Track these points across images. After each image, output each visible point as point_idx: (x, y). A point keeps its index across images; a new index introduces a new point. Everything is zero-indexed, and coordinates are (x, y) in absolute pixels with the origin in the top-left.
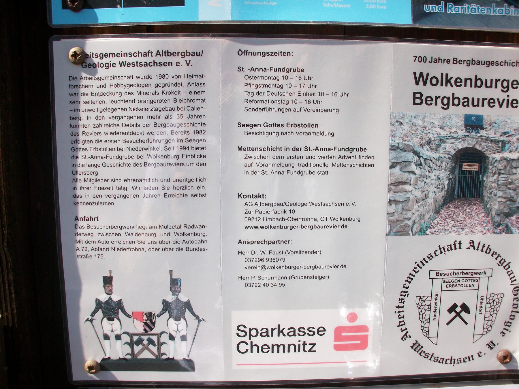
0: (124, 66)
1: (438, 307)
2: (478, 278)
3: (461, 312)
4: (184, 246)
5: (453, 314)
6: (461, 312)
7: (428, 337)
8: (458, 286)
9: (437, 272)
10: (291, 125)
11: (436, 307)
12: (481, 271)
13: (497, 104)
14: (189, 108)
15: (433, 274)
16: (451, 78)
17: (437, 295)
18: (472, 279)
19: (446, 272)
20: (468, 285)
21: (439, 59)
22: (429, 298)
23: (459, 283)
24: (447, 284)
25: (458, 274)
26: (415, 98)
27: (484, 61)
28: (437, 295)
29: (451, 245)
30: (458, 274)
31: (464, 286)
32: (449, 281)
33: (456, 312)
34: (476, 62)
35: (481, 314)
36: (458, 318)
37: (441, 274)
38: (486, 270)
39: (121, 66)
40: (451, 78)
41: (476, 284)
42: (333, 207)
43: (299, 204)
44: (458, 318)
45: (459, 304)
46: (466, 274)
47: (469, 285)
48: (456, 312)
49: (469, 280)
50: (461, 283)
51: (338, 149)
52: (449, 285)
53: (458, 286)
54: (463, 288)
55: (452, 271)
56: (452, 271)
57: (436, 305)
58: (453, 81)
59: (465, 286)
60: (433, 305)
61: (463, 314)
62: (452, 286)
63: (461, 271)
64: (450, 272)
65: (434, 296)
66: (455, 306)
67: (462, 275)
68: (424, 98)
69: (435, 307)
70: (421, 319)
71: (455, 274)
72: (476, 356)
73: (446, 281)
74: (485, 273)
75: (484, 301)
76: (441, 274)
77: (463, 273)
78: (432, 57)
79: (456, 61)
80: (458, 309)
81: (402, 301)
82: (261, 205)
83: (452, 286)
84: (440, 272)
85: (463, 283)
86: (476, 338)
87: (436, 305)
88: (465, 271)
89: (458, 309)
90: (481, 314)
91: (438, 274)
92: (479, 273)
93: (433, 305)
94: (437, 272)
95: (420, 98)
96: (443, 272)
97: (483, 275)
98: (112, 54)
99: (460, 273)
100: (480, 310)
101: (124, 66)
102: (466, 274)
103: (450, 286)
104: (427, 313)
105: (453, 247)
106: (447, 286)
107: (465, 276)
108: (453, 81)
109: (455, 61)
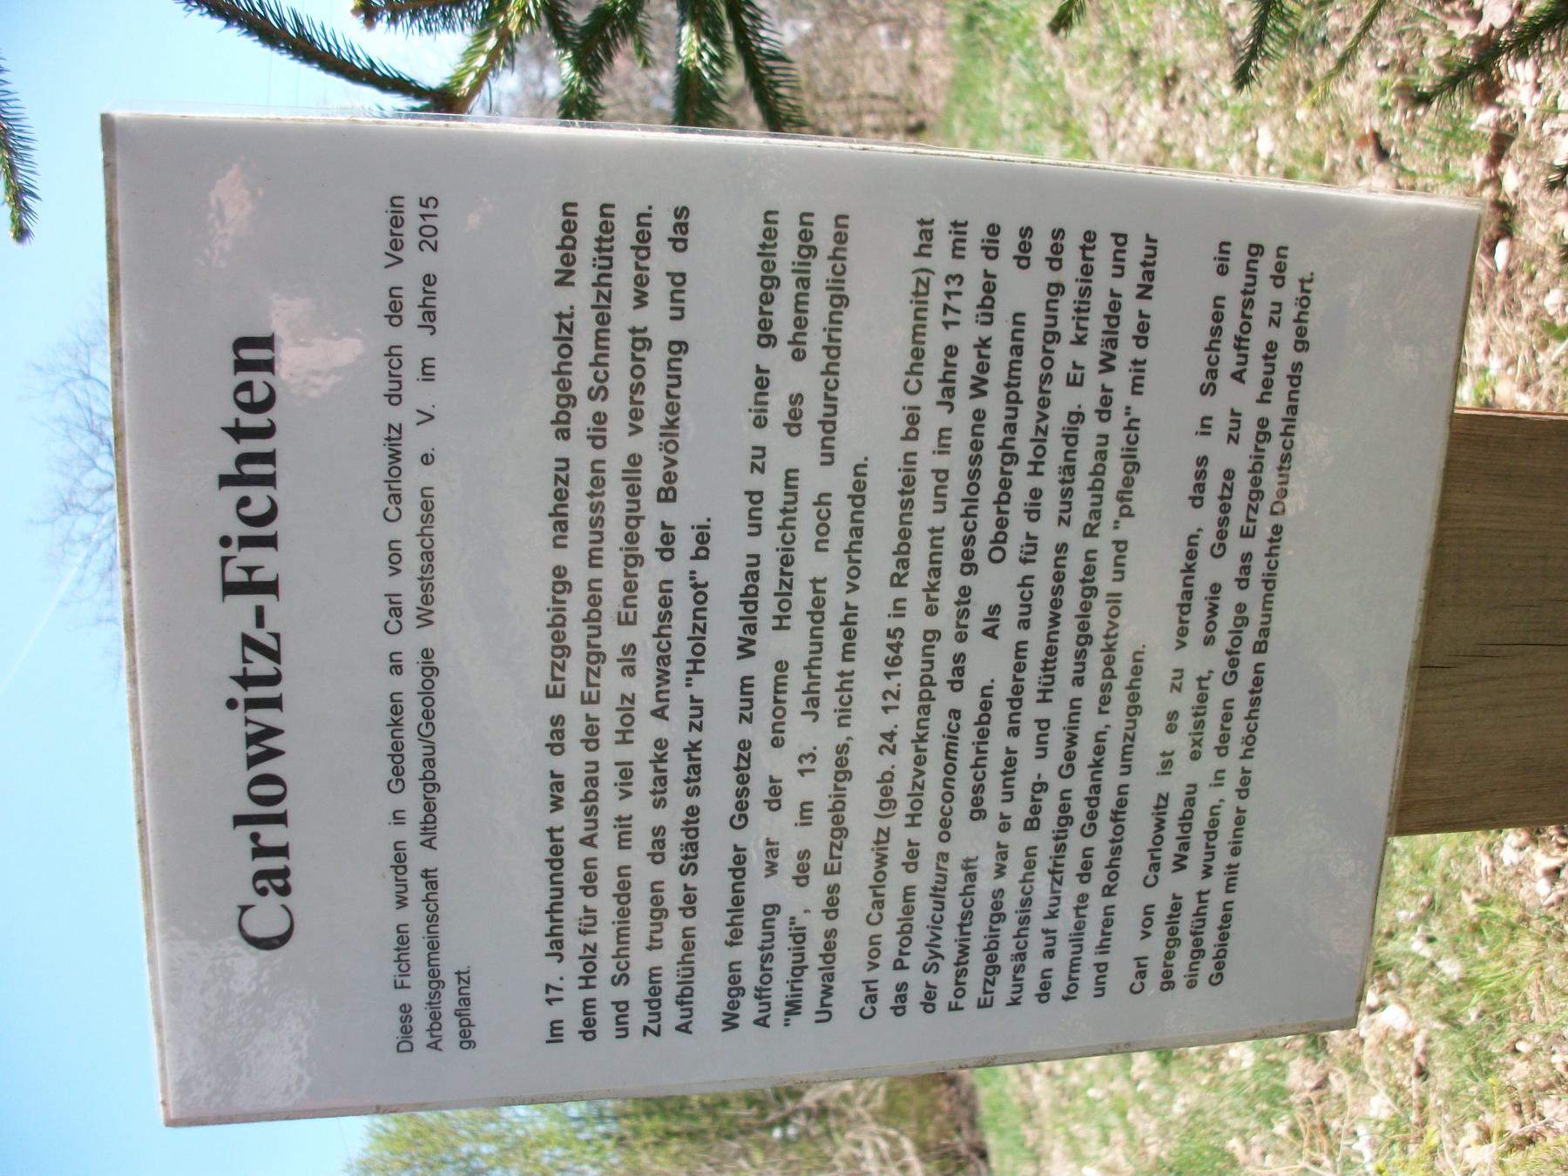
0: (737, 1016)
4: (573, 764)
10: (627, 610)
13: (672, 469)
14: (875, 918)
21: (552, 934)
26: (667, 500)
34: (590, 788)
39: (984, 393)
42: (438, 530)
43: (428, 684)
68: (666, 486)
78: (547, 955)
79: (666, 491)
82: (432, 826)
95: (666, 491)
98: (430, 959)
101: (737, 1016)
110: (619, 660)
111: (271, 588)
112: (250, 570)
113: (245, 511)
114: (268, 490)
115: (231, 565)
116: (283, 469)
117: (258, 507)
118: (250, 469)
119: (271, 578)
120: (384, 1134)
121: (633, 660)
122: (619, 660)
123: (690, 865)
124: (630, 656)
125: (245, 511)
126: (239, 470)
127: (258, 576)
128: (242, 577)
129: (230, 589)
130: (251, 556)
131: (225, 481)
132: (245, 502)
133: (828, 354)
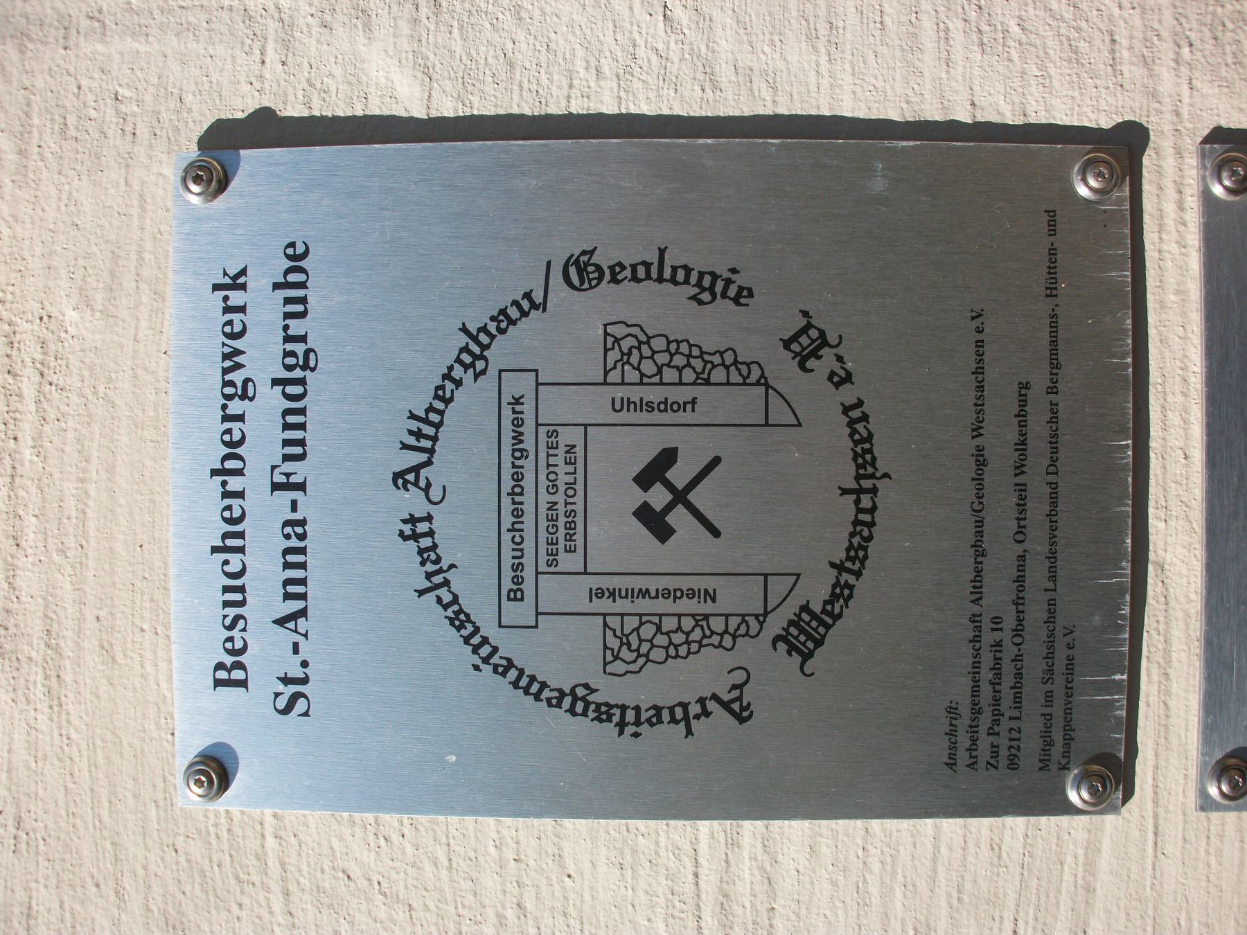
1: (653, 584)
2: (542, 430)
3: (669, 486)
5: (679, 518)
6: (669, 486)
7: (766, 614)
8: (569, 507)
9: (509, 599)
11: (653, 594)
12: (507, 413)
15: (513, 612)
16: (609, 597)
17: (600, 593)
18: (548, 455)
19: (507, 562)
20: (570, 469)
22: (614, 622)
23: (561, 508)
24: (561, 549)
25: (518, 514)
27: (514, 550)
28: (600, 593)
29: (421, 552)
30: (518, 514)
31: (570, 486)
32: (552, 544)
33: (669, 507)
35: (694, 402)
36: (691, 497)
37: (518, 581)
38: (506, 398)
40: (609, 597)
41: (569, 436)
44: (691, 497)
45: (637, 497)
46: (518, 478)
47: (570, 463)
48: (669, 507)
49: (548, 465)
50: (560, 498)
52: (568, 543)
53: (569, 507)
54: (579, 487)
55: (507, 537)
56: (507, 537)
57: (644, 593)
58: (607, 594)
59: (570, 479)
60: (644, 605)
61: (679, 475)
62: (572, 532)
63: (506, 501)
64: (507, 546)
65: (604, 605)
66: (644, 514)
67: (521, 494)
68: (515, 587)
69: (657, 597)
70: (694, 647)
71: (517, 526)
72: (848, 394)
73: (552, 554)
74: (517, 401)
75: (635, 394)
76: (518, 581)
77: (513, 493)
79: (515, 592)
80: (658, 497)
81: (1020, 621)
83: (572, 532)
84: (507, 584)
85: (562, 488)
86: (779, 412)
87: (644, 593)
88: (508, 484)
89: (658, 497)
90: (694, 402)
91: (516, 596)
92: (518, 423)
93: (644, 605)
94: (509, 599)
95: (515, 592)
96: (508, 574)
97: (528, 409)
99: (514, 503)
100: (681, 407)
102: (518, 478)
103: (570, 538)
104: (669, 624)
105: (426, 542)
106: (570, 551)
107: (528, 482)
108: (607, 594)
109: (515, 595)
110: (641, 399)
111: (301, 487)
112: (288, 475)
113: (226, 568)
114: (240, 556)
115: (277, 471)
116: (249, 542)
117: (234, 567)
118: (230, 542)
119: (301, 480)
120: (204, 833)
121: (641, 411)
122: (641, 399)
123: (553, 560)
124: (644, 407)
125: (226, 568)
126: (223, 542)
127: (293, 479)
128: (283, 479)
129: (276, 487)
130: (289, 467)
131: (215, 550)
132: (226, 562)
133: (680, 598)
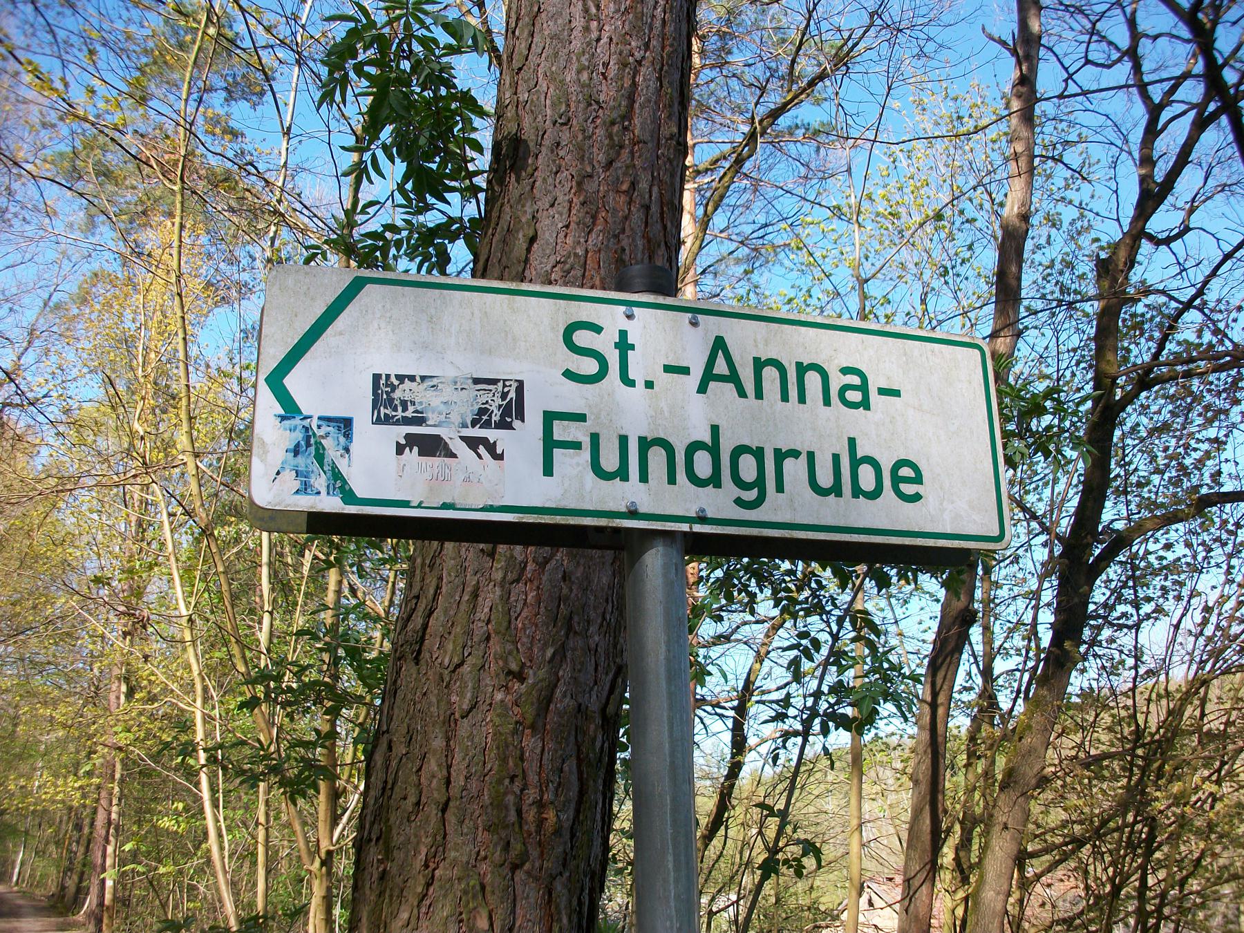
51: (595, 438)
